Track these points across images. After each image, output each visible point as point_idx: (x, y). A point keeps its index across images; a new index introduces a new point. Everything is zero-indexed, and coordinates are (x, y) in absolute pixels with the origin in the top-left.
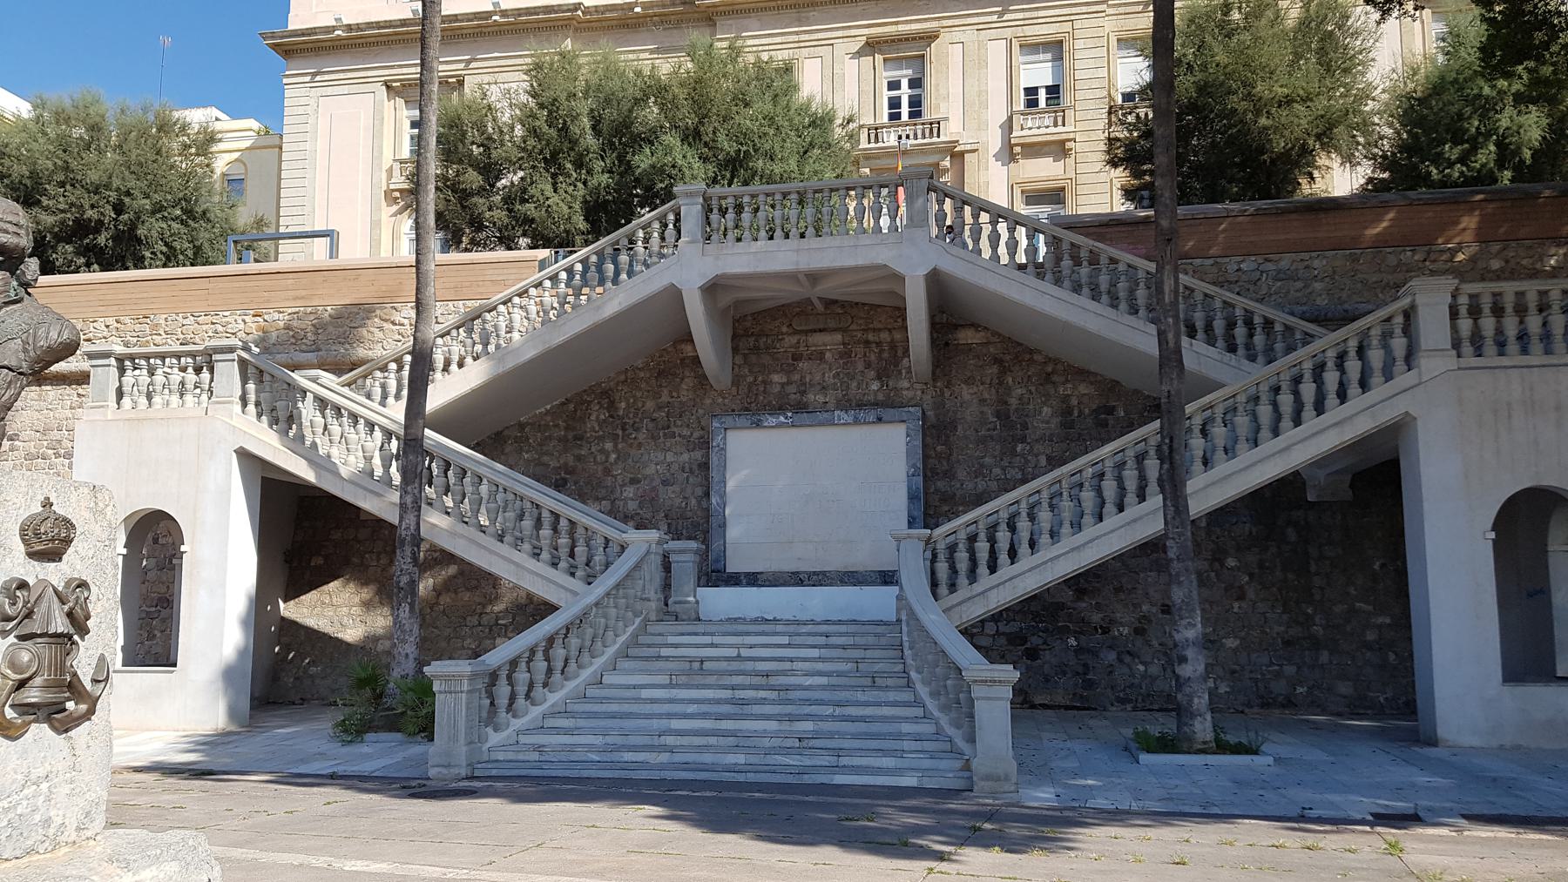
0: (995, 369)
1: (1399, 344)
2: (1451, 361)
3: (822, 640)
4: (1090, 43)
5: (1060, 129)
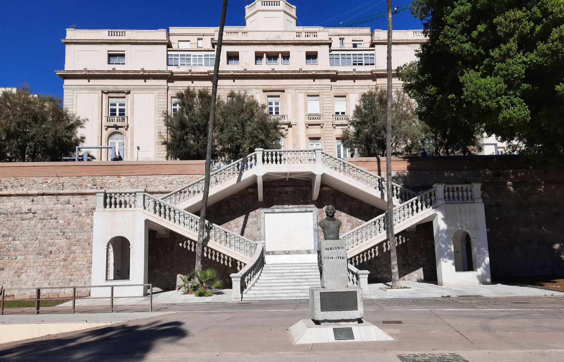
0: (333, 198)
1: (433, 198)
2: (443, 201)
3: (310, 267)
4: (327, 96)
5: (319, 121)
